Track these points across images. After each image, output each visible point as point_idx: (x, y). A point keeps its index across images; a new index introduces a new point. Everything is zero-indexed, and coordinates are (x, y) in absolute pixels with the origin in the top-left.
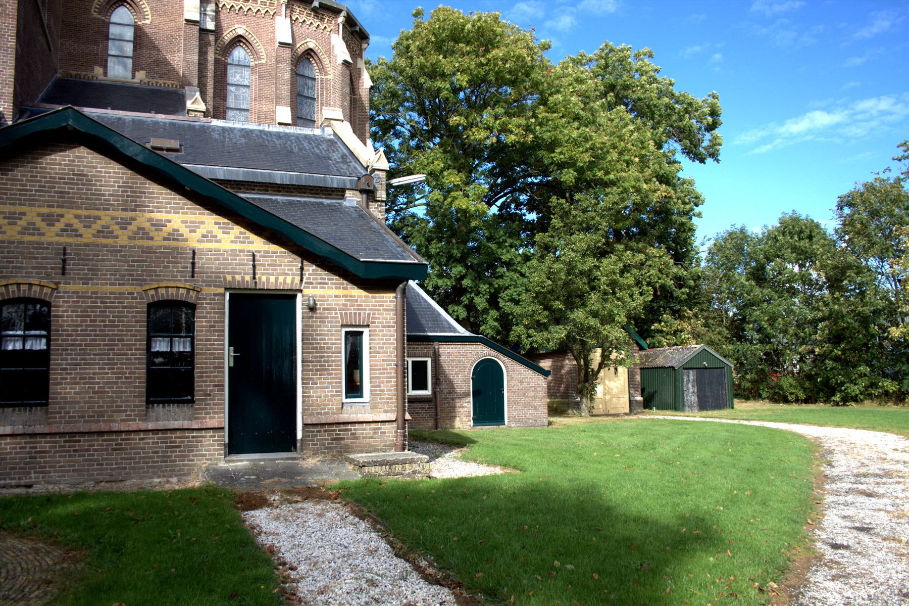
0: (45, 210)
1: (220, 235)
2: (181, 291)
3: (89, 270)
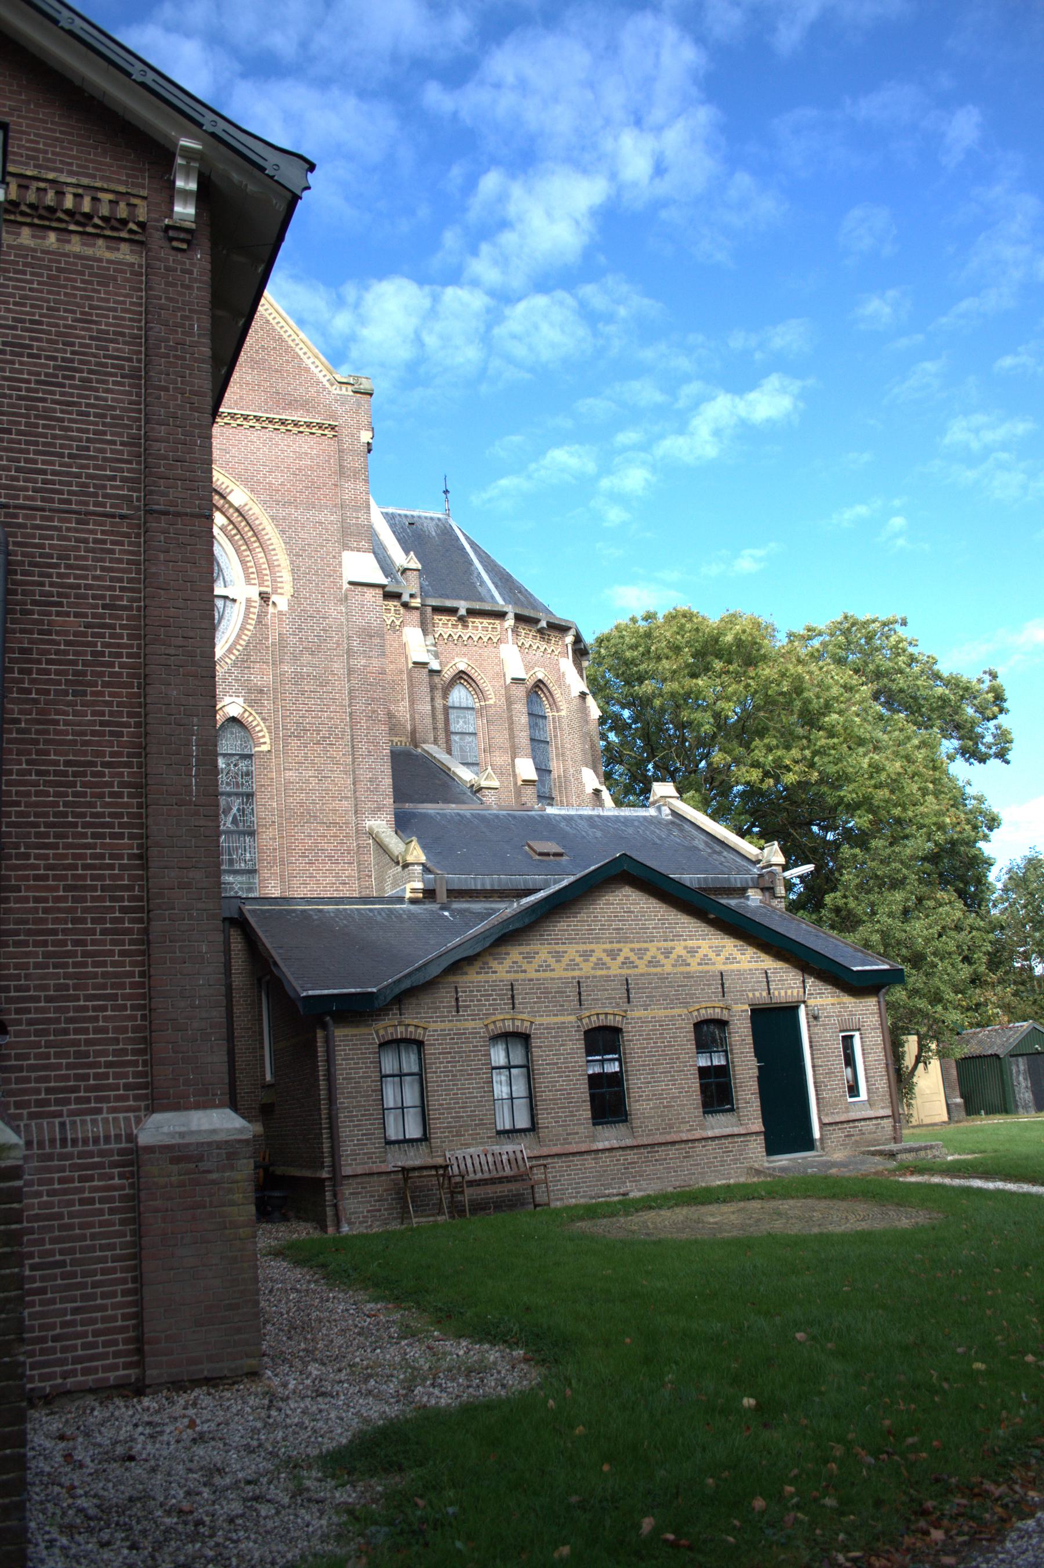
0: (608, 946)
1: (739, 957)
2: (717, 1010)
3: (647, 997)
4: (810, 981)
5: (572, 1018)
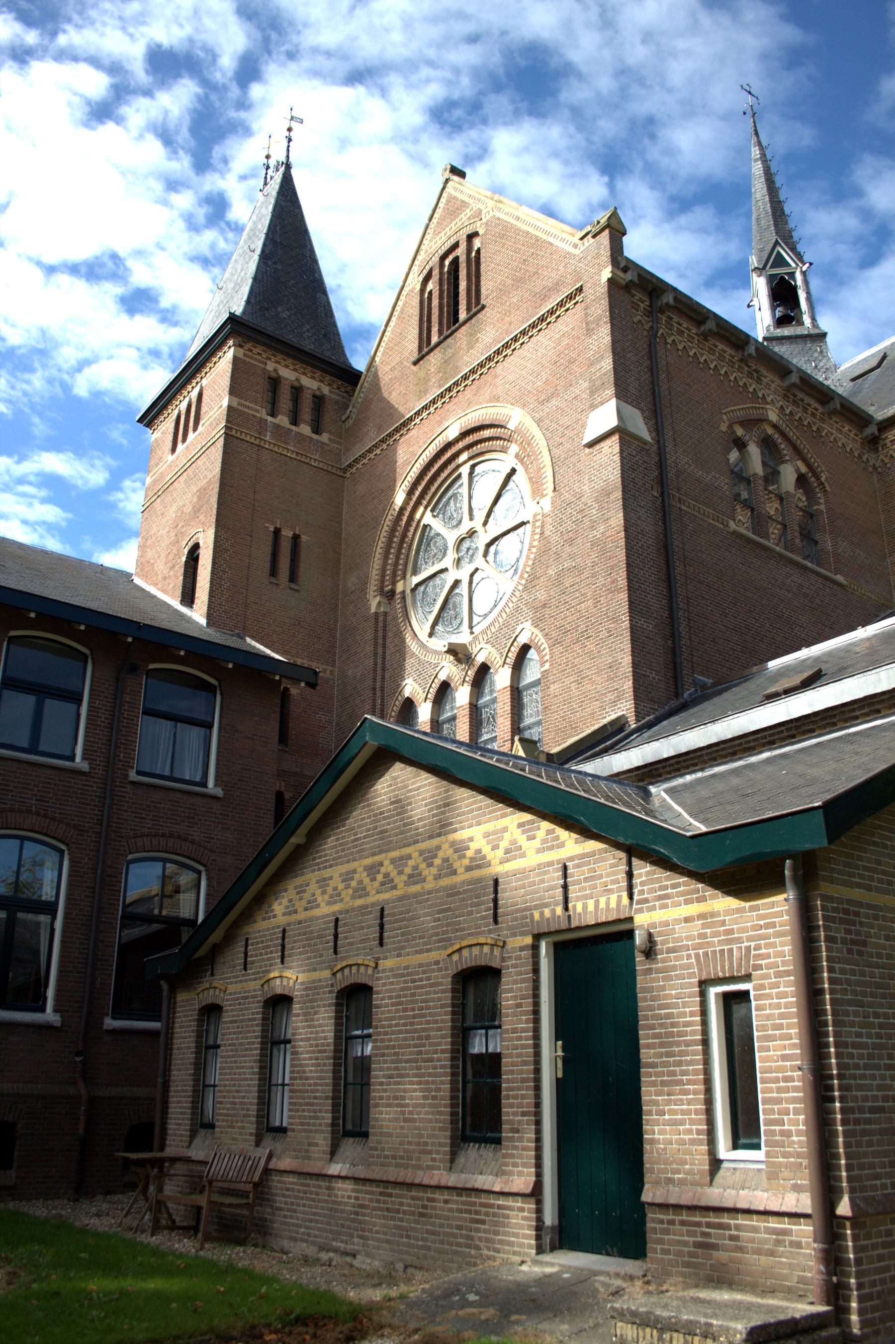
4: (643, 870)
5: (327, 973)
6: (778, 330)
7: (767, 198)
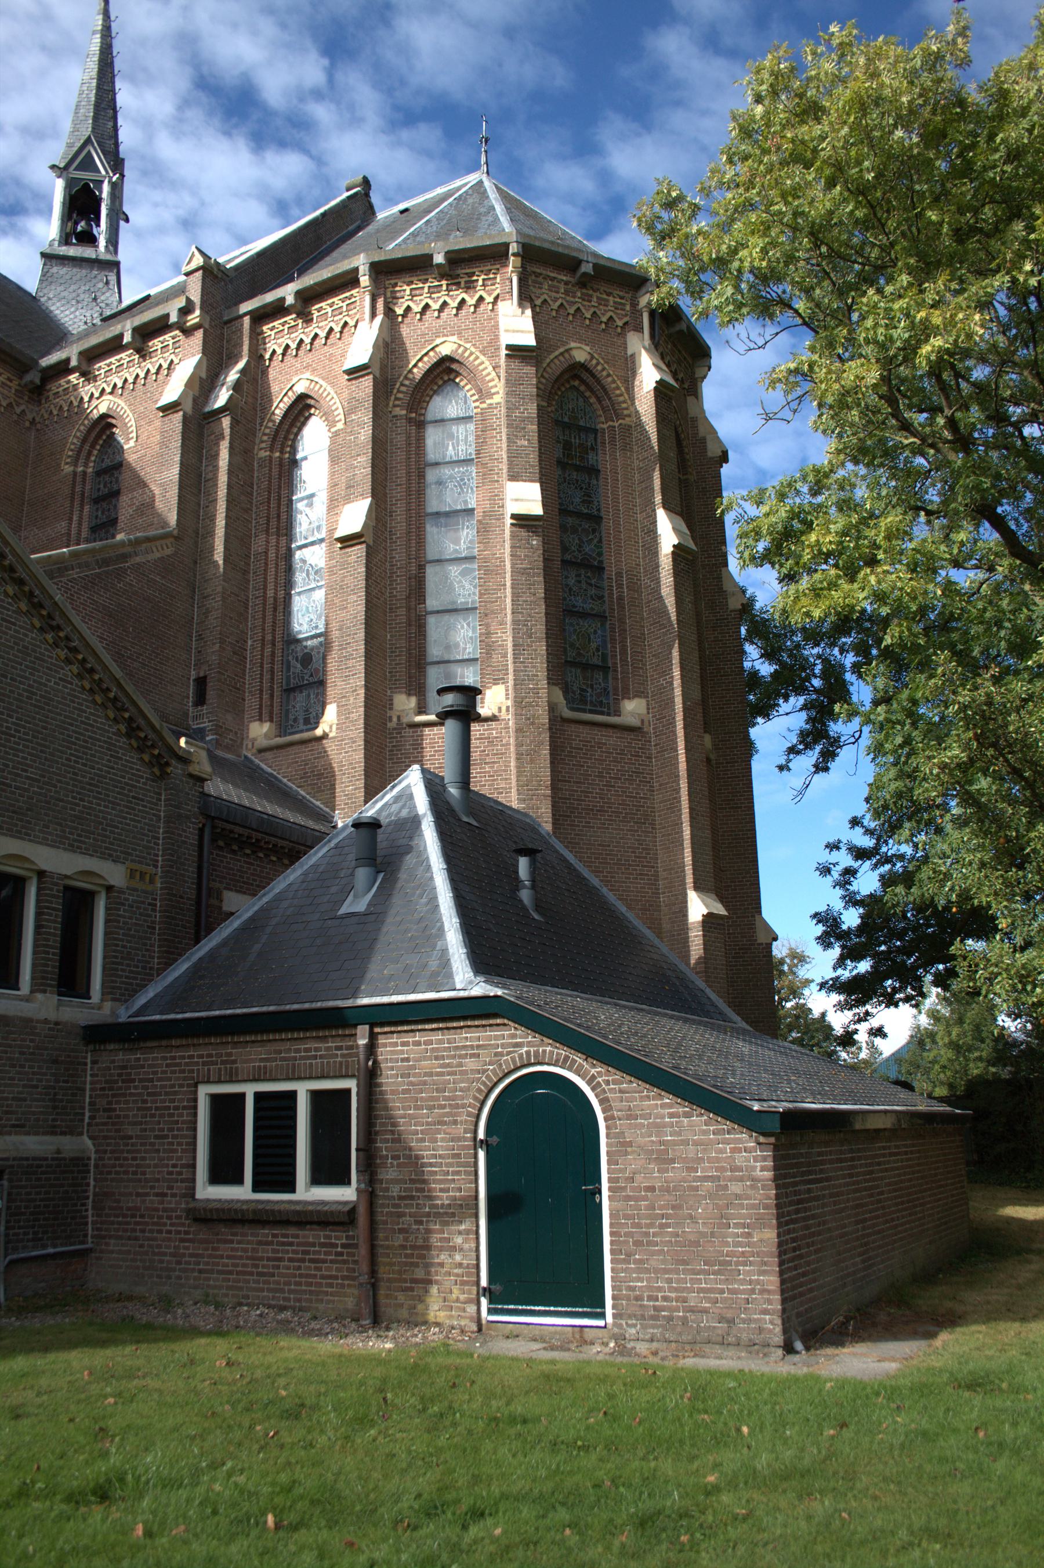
6: (64, 248)
7: (94, 83)
